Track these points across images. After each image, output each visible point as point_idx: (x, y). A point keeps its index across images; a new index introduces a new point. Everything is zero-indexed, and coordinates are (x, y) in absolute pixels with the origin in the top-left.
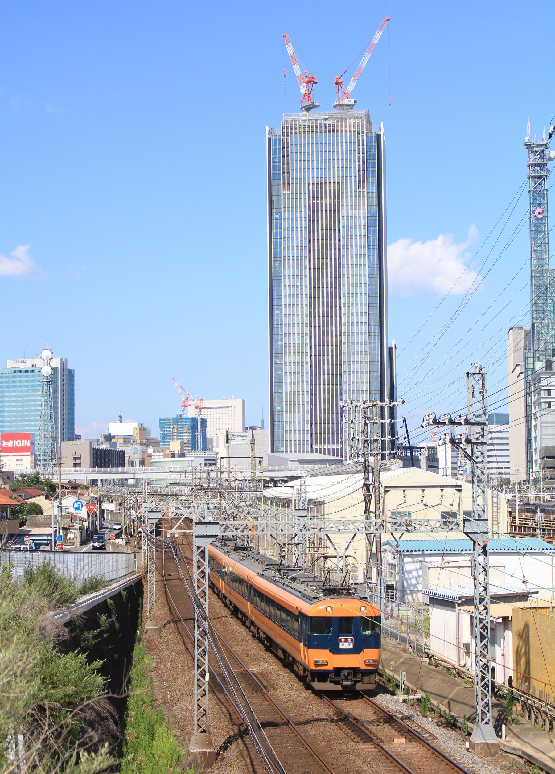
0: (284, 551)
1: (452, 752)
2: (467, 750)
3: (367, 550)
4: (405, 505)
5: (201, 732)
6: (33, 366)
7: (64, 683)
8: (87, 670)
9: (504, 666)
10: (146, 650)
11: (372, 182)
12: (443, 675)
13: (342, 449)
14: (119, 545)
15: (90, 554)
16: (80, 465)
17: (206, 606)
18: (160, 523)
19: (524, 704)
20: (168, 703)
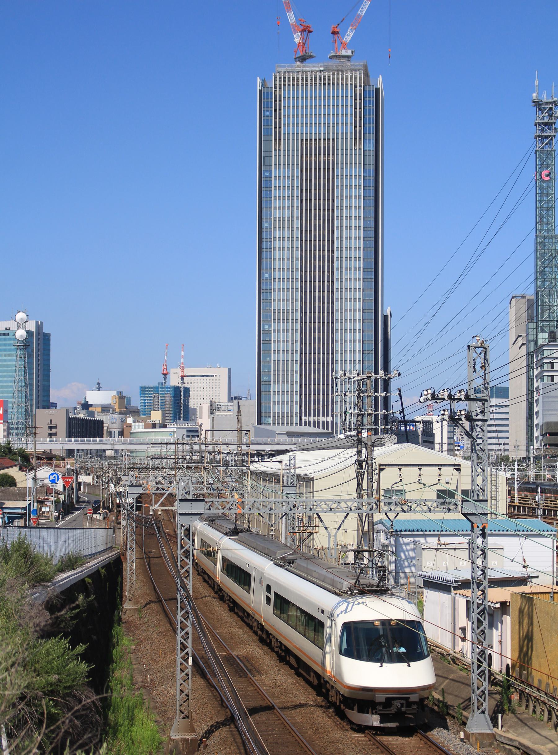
0: (272, 530)
1: (446, 742)
2: (462, 740)
3: (358, 531)
4: (400, 484)
5: (184, 718)
6: (6, 329)
7: (46, 671)
8: (70, 656)
9: (501, 655)
10: (125, 631)
11: (369, 140)
12: (437, 661)
13: (332, 422)
14: (96, 520)
15: (67, 530)
16: (55, 434)
17: (190, 587)
18: (140, 499)
19: (521, 693)
20: (148, 687)
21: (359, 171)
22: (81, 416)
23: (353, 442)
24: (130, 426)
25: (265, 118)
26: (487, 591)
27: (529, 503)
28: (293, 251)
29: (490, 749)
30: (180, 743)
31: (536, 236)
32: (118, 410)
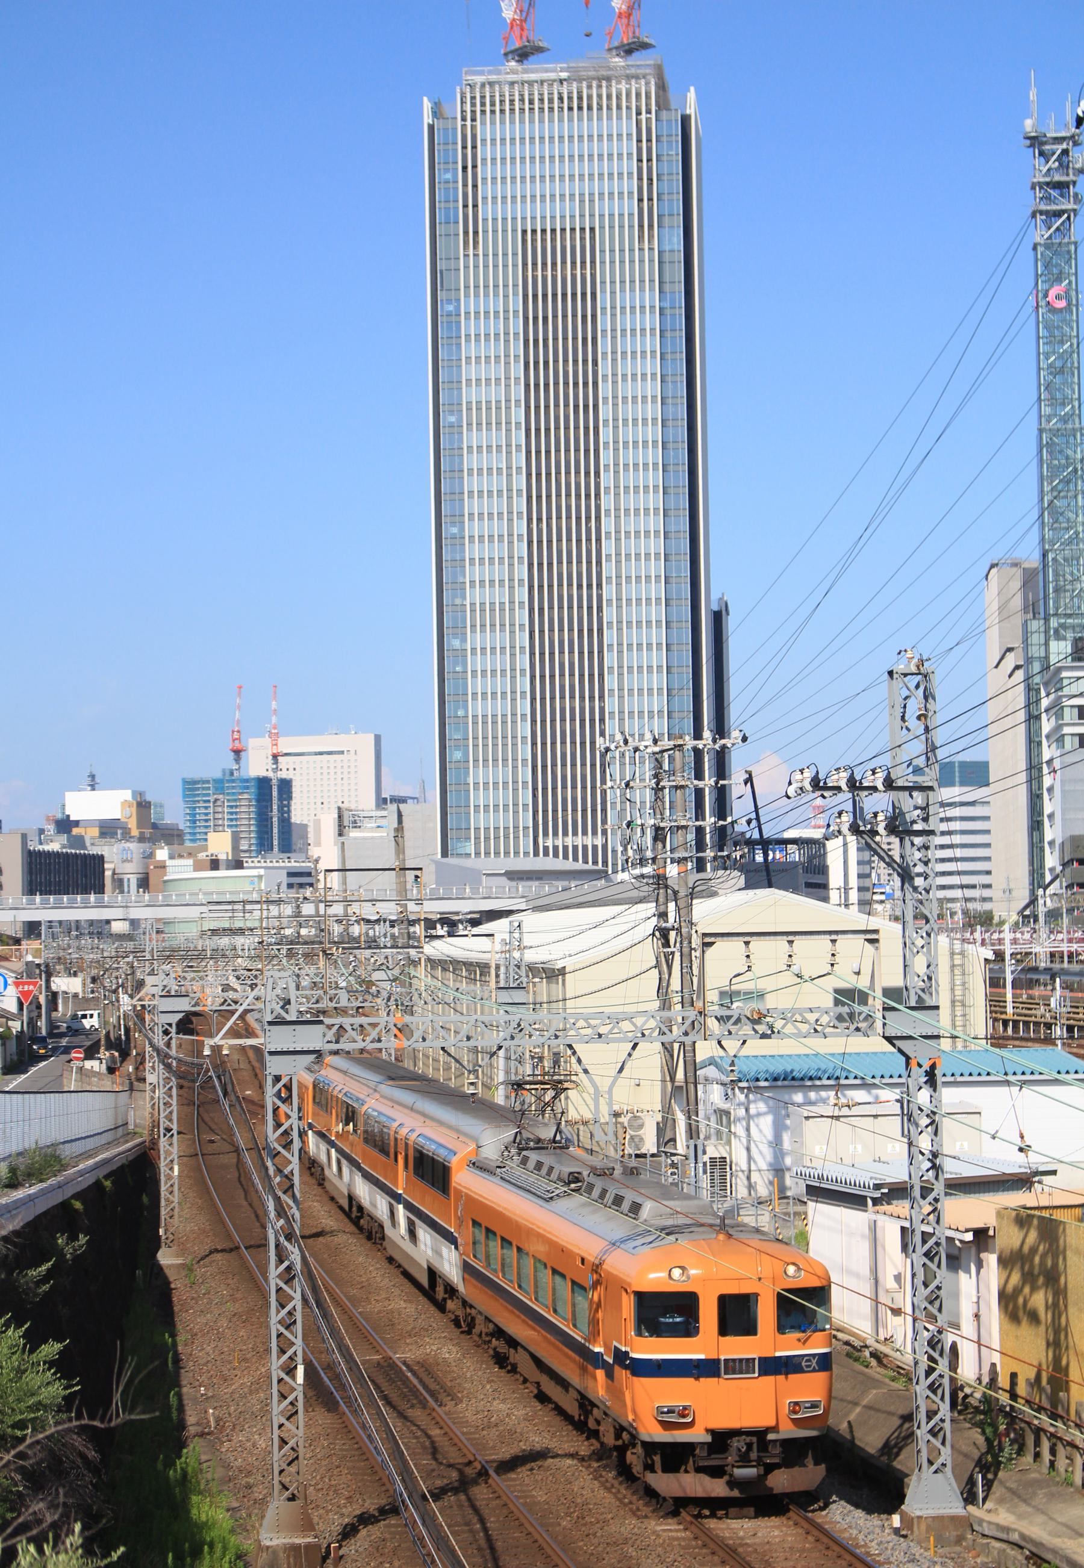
1: (861, 1537)
3: (663, 1081)
5: (289, 1499)
9: (979, 1344)
13: (605, 847)
14: (93, 1073)
15: (27, 1096)
21: (651, 297)
22: (54, 846)
23: (646, 888)
24: (162, 866)
25: (442, 186)
26: (943, 1205)
27: (1038, 1013)
28: (509, 475)
29: (958, 1549)
30: (281, 1554)
31: (1041, 431)
32: (135, 832)
